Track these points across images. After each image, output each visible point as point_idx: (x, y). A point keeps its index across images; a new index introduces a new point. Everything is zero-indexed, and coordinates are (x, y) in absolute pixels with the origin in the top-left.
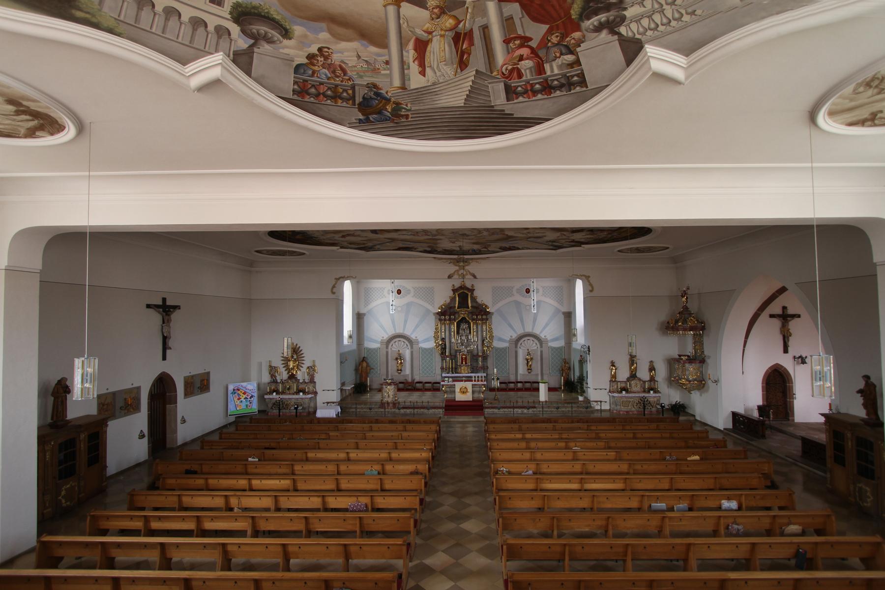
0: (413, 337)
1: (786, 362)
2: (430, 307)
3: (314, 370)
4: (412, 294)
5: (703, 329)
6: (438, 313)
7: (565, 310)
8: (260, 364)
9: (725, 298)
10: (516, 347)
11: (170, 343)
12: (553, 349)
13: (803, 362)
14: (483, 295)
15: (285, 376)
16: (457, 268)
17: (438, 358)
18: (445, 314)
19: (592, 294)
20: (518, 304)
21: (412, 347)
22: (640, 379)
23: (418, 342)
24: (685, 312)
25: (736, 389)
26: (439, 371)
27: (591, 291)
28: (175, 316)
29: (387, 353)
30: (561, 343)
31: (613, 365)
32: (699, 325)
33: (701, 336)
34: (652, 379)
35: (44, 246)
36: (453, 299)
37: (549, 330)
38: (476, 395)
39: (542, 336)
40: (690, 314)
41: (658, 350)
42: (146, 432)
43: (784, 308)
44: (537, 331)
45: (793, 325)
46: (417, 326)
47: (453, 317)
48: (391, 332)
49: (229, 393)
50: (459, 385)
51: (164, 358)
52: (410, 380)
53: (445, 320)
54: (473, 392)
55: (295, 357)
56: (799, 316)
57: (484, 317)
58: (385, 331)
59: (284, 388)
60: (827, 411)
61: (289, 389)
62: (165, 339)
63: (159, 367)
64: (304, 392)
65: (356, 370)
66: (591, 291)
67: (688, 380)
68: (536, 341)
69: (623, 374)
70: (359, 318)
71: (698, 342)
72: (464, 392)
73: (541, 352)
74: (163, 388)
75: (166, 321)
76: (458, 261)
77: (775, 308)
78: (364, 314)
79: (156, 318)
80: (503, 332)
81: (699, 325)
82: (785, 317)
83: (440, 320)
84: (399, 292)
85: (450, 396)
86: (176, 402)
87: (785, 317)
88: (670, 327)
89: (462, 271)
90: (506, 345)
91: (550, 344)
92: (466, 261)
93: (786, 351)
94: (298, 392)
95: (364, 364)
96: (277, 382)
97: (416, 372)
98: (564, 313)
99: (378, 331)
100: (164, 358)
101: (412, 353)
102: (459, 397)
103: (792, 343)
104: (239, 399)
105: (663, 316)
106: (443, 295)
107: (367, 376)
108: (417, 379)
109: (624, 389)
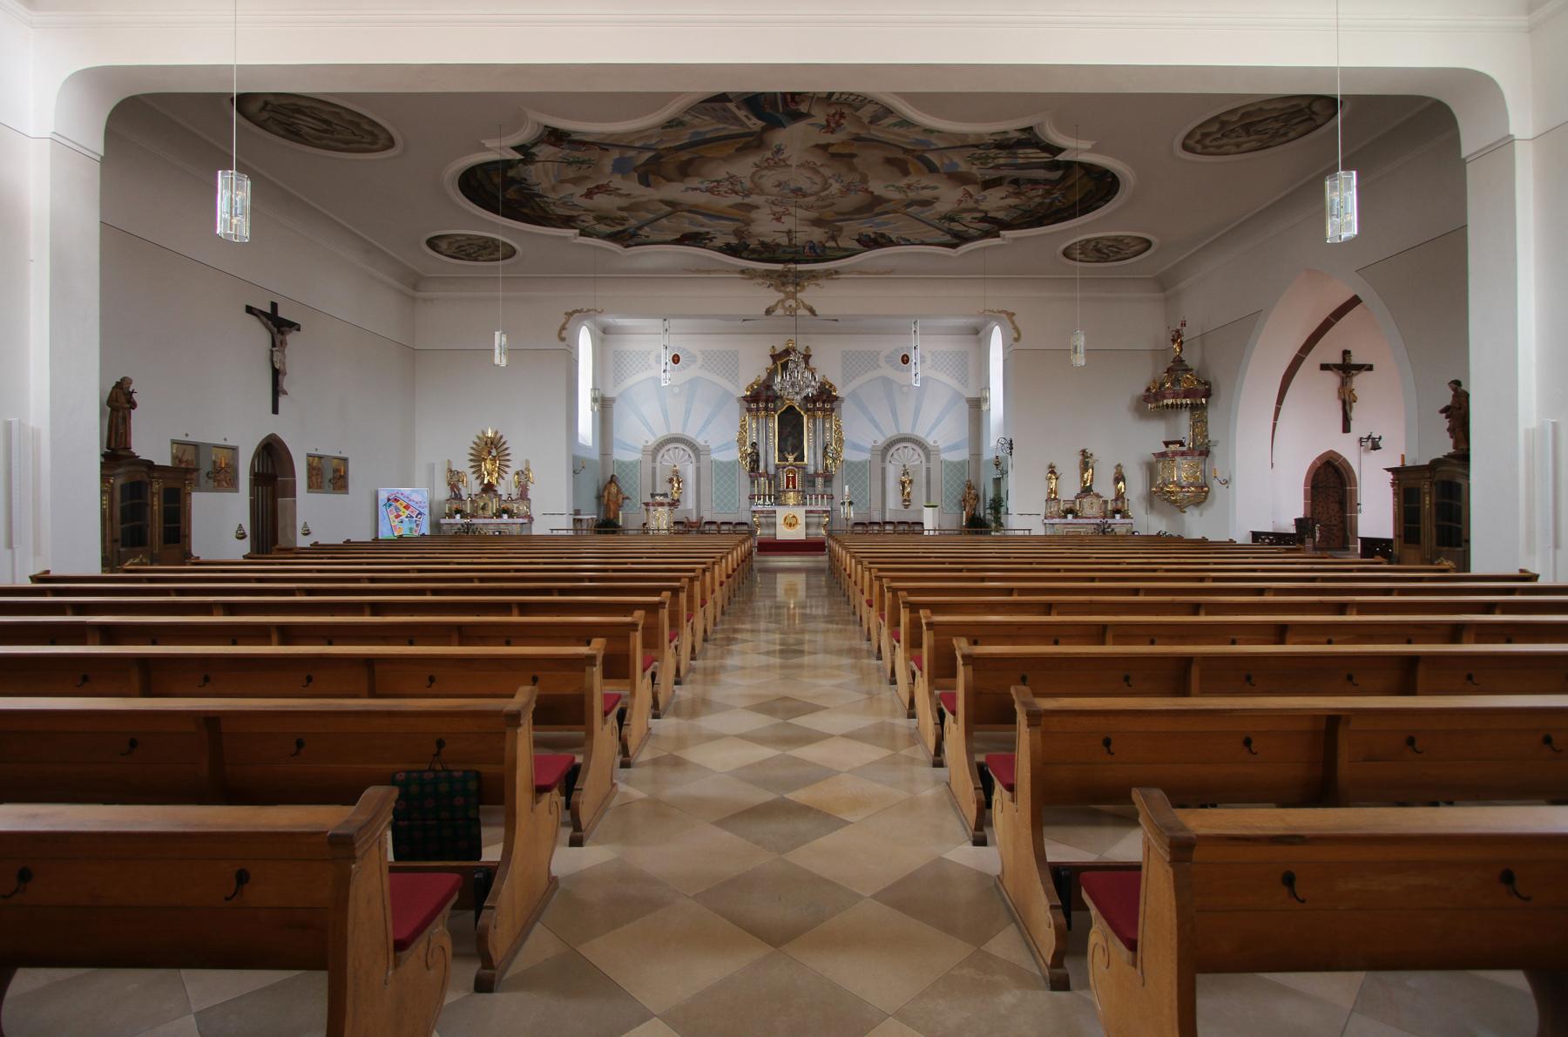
0: (700, 441)
1: (1347, 447)
2: (730, 387)
3: (527, 477)
4: (700, 361)
5: (1207, 394)
6: (745, 398)
7: (972, 395)
8: (432, 468)
9: (1241, 331)
10: (883, 460)
11: (286, 383)
12: (949, 464)
13: (1376, 447)
14: (829, 364)
15: (476, 488)
16: (782, 296)
17: (745, 479)
19: (1018, 345)
20: (887, 382)
21: (698, 460)
22: (1098, 496)
23: (708, 451)
24: (1178, 367)
25: (1262, 486)
26: (745, 501)
27: (1016, 340)
28: (292, 338)
29: (654, 469)
30: (963, 455)
31: (1052, 472)
32: (1201, 388)
33: (1203, 407)
34: (1120, 496)
35: (119, 100)
37: (942, 431)
38: (813, 531)
39: (930, 441)
40: (1187, 370)
41: (1128, 444)
42: (247, 529)
43: (1346, 353)
44: (920, 433)
45: (1360, 382)
46: (708, 422)
47: (771, 405)
48: (662, 433)
49: (381, 504)
51: (275, 410)
52: (694, 519)
53: (758, 410)
54: (808, 525)
55: (494, 453)
56: (1370, 368)
57: (827, 406)
58: (651, 430)
59: (475, 509)
60: (1398, 464)
61: (483, 508)
62: (276, 374)
63: (269, 425)
64: (511, 514)
65: (599, 497)
66: (1016, 340)
67: (1177, 484)
68: (919, 451)
69: (1069, 489)
70: (604, 405)
71: (1200, 424)
72: (791, 521)
73: (928, 470)
74: (272, 454)
75: (277, 343)
76: (780, 280)
77: (1328, 351)
78: (613, 400)
79: (260, 335)
80: (859, 432)
81: (1201, 388)
82: (1347, 369)
83: (749, 410)
84: (676, 359)
86: (294, 495)
87: (1347, 369)
88: (1153, 402)
89: (791, 302)
90: (866, 456)
91: (945, 456)
92: (799, 280)
93: (1346, 428)
94: (499, 514)
95: (614, 489)
96: (461, 499)
97: (705, 505)
98: (969, 401)
99: (638, 432)
100: (275, 410)
102: (784, 533)
103: (1356, 414)
104: (398, 516)
105: (1141, 378)
106: (754, 367)
107: (619, 507)
108: (707, 518)
109: (1071, 511)
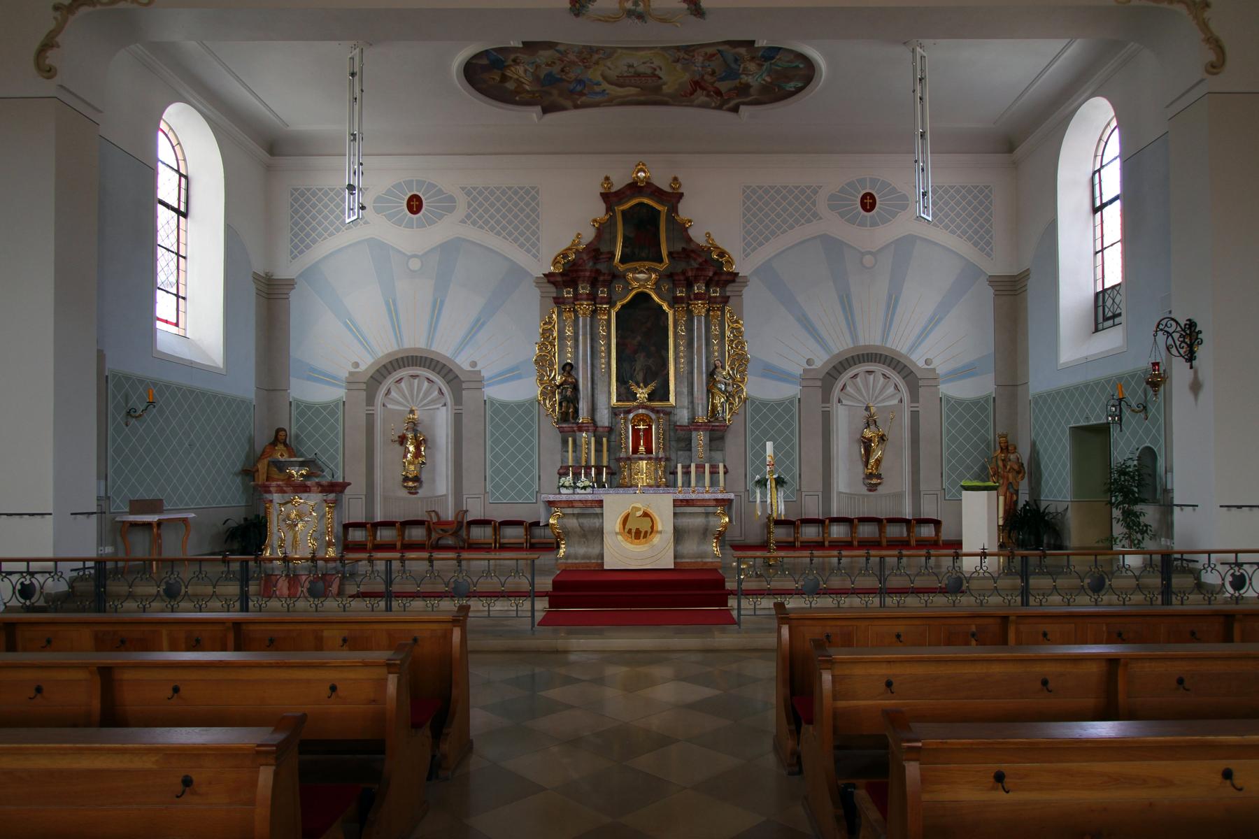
0: (463, 362)
10: (826, 398)
18: (576, 278)
21: (458, 400)
23: (478, 381)
36: (604, 230)
38: (691, 547)
46: (477, 326)
50: (616, 505)
54: (679, 534)
90: (791, 390)
97: (471, 485)
101: (458, 419)
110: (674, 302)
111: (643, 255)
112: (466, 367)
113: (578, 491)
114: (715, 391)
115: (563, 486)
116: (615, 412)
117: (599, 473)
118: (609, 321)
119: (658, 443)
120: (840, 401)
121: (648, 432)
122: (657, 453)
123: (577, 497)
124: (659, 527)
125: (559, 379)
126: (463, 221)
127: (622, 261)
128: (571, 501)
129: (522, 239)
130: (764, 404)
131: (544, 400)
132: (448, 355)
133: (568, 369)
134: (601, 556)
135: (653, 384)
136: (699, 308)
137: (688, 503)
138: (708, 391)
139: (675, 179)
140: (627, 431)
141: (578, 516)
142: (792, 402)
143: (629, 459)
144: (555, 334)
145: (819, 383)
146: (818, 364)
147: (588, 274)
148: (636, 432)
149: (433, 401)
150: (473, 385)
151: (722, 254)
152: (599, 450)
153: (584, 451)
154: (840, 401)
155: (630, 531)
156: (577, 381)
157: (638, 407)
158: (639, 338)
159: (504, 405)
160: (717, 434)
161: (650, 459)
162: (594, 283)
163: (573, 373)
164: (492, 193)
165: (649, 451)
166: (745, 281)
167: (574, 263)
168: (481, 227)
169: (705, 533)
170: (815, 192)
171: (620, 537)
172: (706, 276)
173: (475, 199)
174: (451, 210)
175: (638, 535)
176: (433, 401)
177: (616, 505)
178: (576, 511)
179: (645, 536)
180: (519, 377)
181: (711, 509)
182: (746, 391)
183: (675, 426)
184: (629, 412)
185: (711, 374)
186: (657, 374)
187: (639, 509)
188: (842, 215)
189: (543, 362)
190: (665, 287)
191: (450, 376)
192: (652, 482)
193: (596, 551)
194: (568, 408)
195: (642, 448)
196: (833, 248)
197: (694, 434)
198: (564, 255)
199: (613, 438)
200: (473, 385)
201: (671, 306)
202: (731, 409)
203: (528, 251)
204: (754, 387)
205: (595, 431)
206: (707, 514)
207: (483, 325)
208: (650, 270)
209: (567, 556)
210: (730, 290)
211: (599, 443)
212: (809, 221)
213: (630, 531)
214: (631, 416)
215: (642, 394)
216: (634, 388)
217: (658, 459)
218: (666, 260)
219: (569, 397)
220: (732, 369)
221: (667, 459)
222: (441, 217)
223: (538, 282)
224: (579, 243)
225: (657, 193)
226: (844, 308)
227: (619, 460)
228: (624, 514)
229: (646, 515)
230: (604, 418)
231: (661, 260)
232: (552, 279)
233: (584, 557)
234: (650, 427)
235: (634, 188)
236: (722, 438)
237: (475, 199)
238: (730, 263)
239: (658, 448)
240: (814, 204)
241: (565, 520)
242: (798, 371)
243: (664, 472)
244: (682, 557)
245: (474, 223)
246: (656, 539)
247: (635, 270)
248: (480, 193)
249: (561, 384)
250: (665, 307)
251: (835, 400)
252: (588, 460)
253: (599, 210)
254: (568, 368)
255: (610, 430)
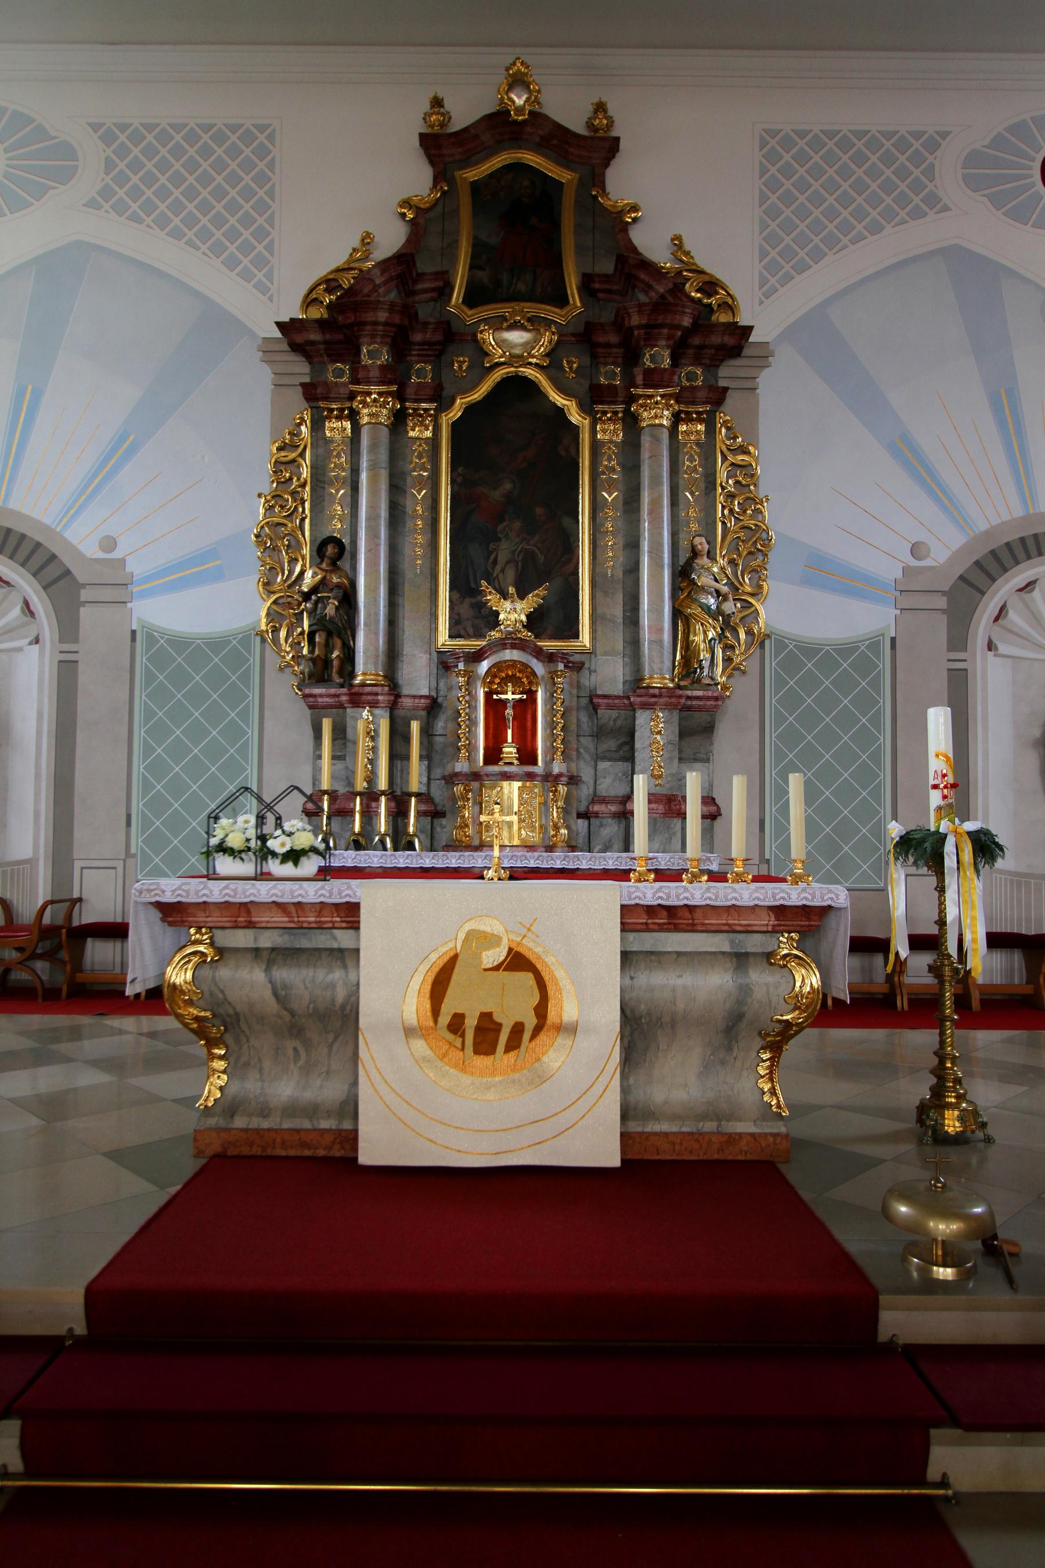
0: (81, 538)
4: (89, 178)
10: (958, 640)
14: (687, 192)
17: (282, 701)
18: (354, 337)
21: (68, 628)
23: (119, 586)
36: (422, 221)
38: (681, 1084)
46: (121, 450)
50: (408, 930)
54: (640, 1031)
85: (286, 1089)
90: (867, 619)
97: (95, 838)
101: (67, 674)
110: (593, 399)
111: (521, 287)
112: (91, 550)
113: (274, 867)
114: (693, 610)
115: (223, 848)
116: (445, 663)
117: (398, 813)
118: (434, 443)
119: (551, 737)
120: (990, 646)
121: (526, 707)
122: (549, 763)
123: (263, 892)
124: (567, 1007)
125: (309, 579)
126: (92, 204)
127: (472, 299)
128: (245, 907)
129: (219, 207)
130: (809, 650)
131: (276, 630)
132: (47, 520)
133: (333, 552)
134: (350, 1107)
135: (541, 591)
136: (657, 414)
137: (675, 918)
138: (677, 614)
139: (600, 107)
140: (472, 706)
141: (272, 957)
142: (874, 645)
143: (476, 776)
144: (305, 473)
145: (942, 602)
146: (939, 555)
147: (382, 316)
148: (494, 707)
149: (9, 631)
150: (107, 594)
151: (711, 286)
152: (398, 755)
153: (361, 760)
154: (990, 646)
155: (456, 1025)
156: (353, 584)
157: (502, 644)
158: (508, 486)
159: (179, 643)
160: (697, 724)
161: (530, 776)
162: (400, 345)
163: (345, 564)
164: (164, 138)
165: (527, 756)
166: (764, 356)
167: (350, 292)
168: (135, 218)
169: (733, 1028)
170: (932, 146)
171: (420, 1046)
172: (675, 338)
173: (123, 152)
174: (65, 176)
175: (486, 1035)
176: (9, 631)
177: (408, 930)
178: (267, 940)
179: (514, 1043)
180: (218, 576)
181: (754, 943)
182: (767, 615)
183: (592, 696)
184: (477, 656)
185: (683, 575)
186: (548, 567)
187: (490, 940)
188: (996, 201)
189: (273, 539)
190: (571, 364)
191: (52, 571)
192: (535, 837)
193: (332, 1091)
194: (328, 647)
195: (510, 750)
196: (975, 280)
197: (642, 718)
198: (330, 283)
199: (440, 725)
200: (107, 594)
201: (585, 408)
202: (728, 660)
203: (246, 276)
204: (783, 609)
205: (393, 707)
206: (740, 959)
207: (133, 450)
208: (535, 324)
209: (229, 1106)
210: (727, 373)
211: (399, 736)
212: (917, 214)
213: (456, 1025)
214: (484, 666)
215: (512, 613)
216: (492, 598)
217: (550, 779)
218: (575, 299)
219: (332, 622)
220: (732, 562)
221: (573, 780)
222: (40, 193)
223: (267, 349)
224: (366, 258)
225: (556, 139)
226: (1001, 423)
227: (451, 779)
228: (436, 958)
229: (517, 961)
230: (418, 677)
231: (561, 300)
232: (299, 339)
233: (292, 1110)
234: (532, 695)
235: (500, 126)
236: (709, 729)
237: (123, 152)
238: (729, 306)
239: (551, 751)
240: (930, 172)
241: (224, 973)
242: (890, 571)
243: (565, 811)
244: (649, 1114)
245: (120, 209)
246: (555, 1056)
247: (499, 324)
248: (136, 138)
249: (314, 590)
250: (575, 417)
251: (981, 642)
252: (371, 779)
253: (417, 180)
254: (330, 550)
255: (433, 706)
